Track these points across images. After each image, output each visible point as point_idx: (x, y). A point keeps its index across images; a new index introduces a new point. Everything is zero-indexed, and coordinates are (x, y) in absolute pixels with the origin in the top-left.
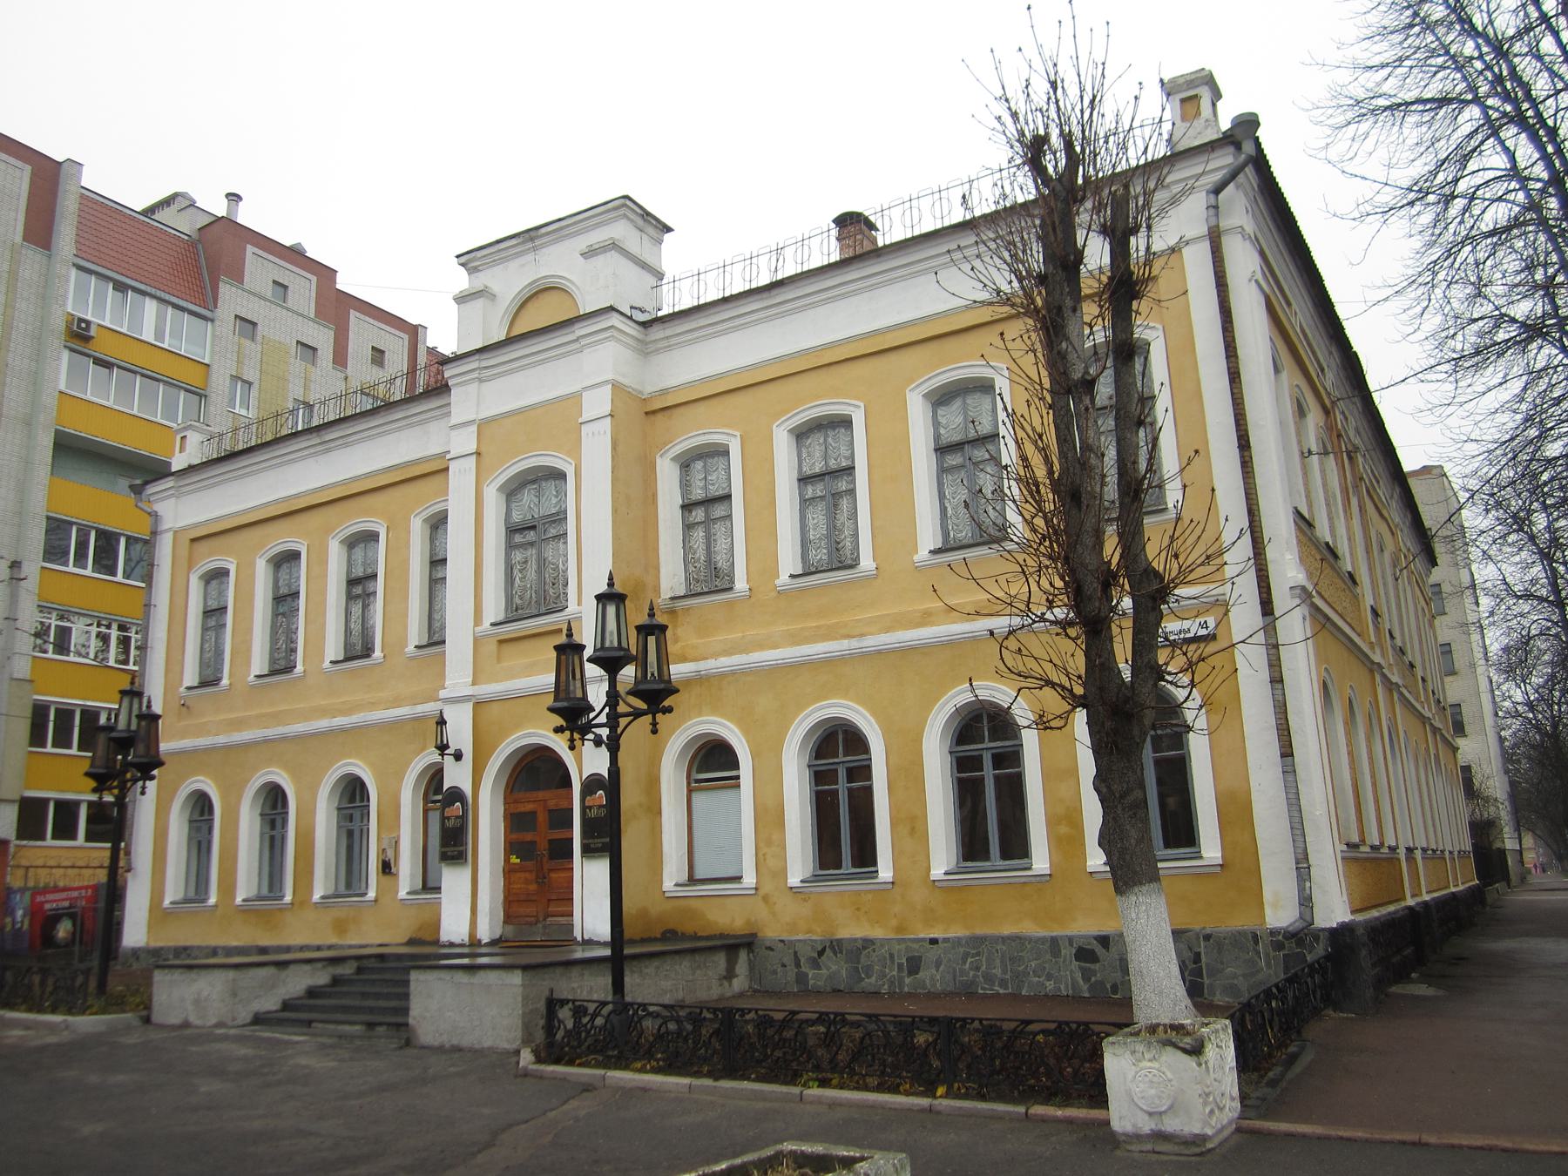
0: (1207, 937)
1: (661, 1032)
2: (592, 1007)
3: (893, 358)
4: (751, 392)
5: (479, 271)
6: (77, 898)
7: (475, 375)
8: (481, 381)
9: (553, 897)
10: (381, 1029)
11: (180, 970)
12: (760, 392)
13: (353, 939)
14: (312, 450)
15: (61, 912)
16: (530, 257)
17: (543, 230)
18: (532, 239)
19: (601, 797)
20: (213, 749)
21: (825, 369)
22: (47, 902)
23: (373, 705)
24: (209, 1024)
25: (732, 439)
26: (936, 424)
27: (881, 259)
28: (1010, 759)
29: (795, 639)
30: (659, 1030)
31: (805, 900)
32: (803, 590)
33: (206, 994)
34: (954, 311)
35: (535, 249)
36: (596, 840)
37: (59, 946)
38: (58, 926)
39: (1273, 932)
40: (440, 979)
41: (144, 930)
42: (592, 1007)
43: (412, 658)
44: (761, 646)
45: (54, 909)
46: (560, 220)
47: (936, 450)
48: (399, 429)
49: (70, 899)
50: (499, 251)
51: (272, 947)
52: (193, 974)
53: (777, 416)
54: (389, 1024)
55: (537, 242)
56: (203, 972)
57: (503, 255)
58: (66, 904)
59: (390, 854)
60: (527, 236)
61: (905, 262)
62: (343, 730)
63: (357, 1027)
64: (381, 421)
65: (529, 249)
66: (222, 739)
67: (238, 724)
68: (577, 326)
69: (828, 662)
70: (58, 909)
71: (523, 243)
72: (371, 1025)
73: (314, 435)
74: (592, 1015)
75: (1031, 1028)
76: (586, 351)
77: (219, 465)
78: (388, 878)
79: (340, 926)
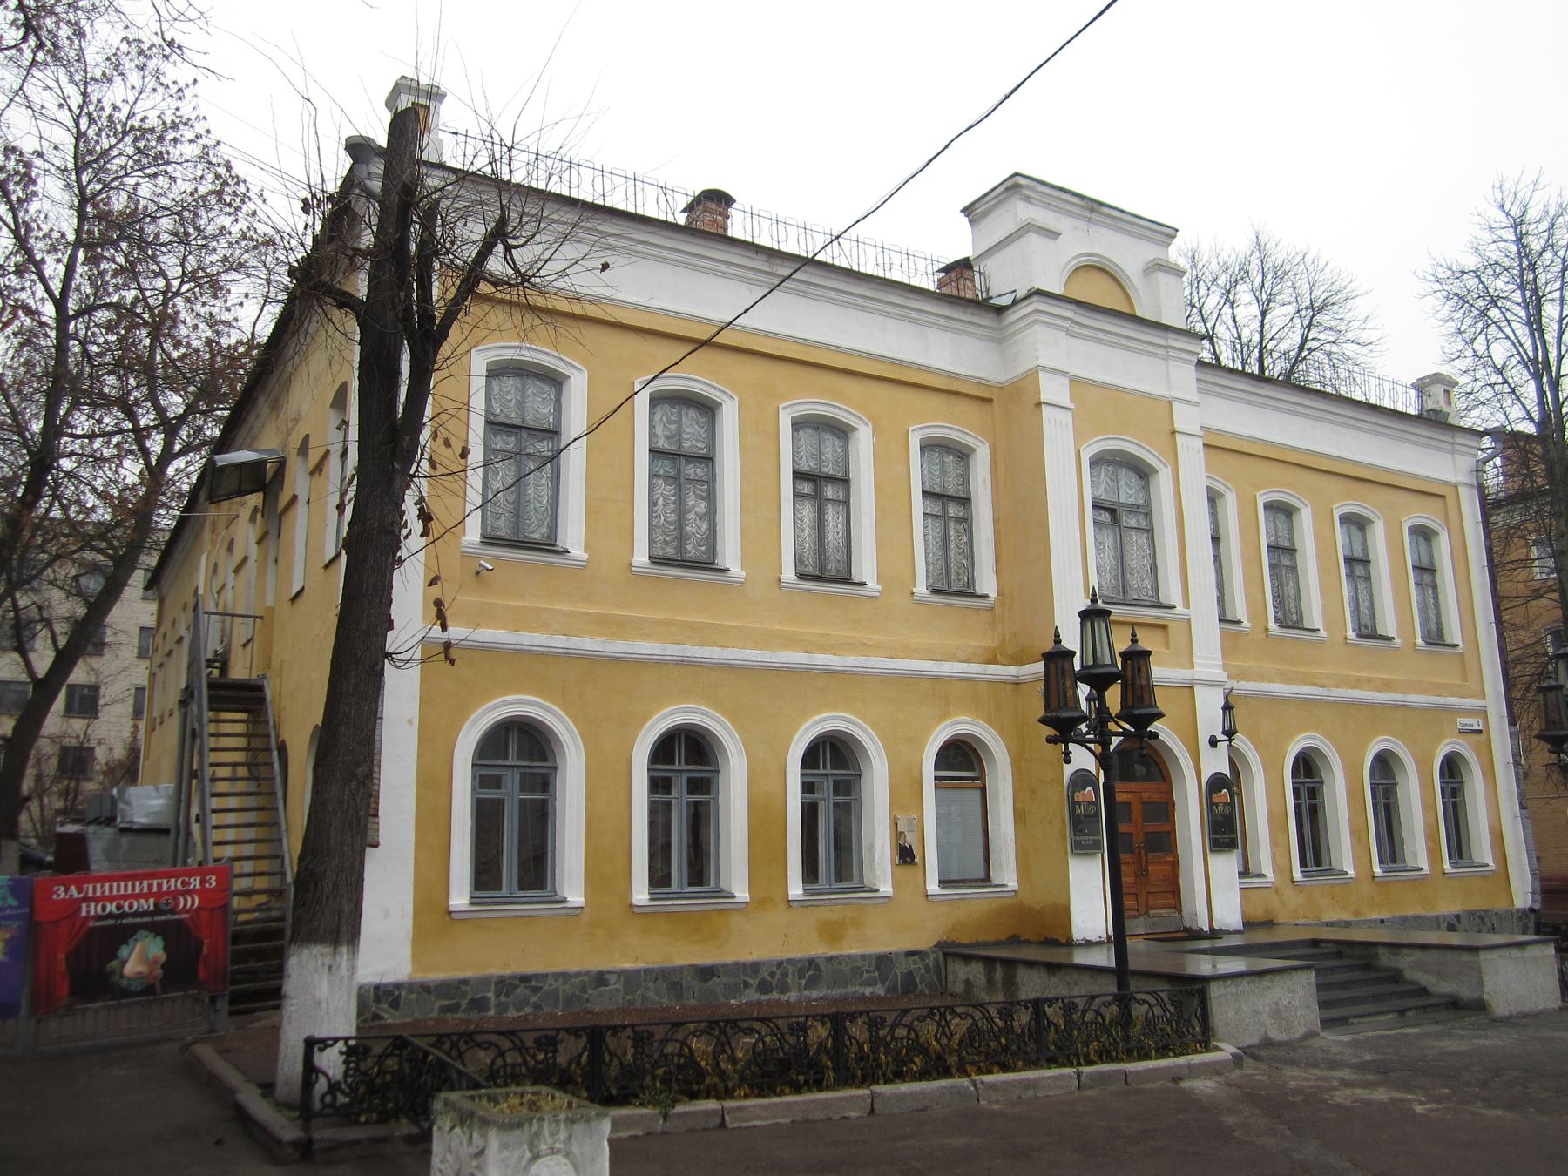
0: (1496, 914)
1: (495, 1067)
2: (1081, 1003)
3: (1322, 477)
4: (1239, 457)
5: (1030, 202)
6: (175, 894)
7: (1066, 324)
8: (1069, 333)
9: (1153, 889)
10: (1409, 1014)
11: (1247, 979)
12: (1246, 460)
13: (852, 947)
14: (749, 275)
15: (130, 920)
16: (1083, 225)
17: (1105, 210)
18: (1092, 210)
19: (1089, 793)
20: (565, 656)
21: (1311, 472)
22: (86, 899)
23: (867, 648)
24: (1297, 1036)
25: (576, 372)
26: (1290, 530)
27: (1326, 401)
28: (543, 781)
29: (1287, 680)
30: (493, 1062)
31: (1301, 892)
32: (1282, 638)
33: (1285, 1003)
34: (913, 366)
35: (1090, 220)
36: (1087, 838)
37: (125, 993)
38: (124, 951)
39: (1518, 910)
40: (1501, 956)
41: (406, 952)
42: (890, 1018)
43: (920, 603)
44: (1261, 678)
45: (111, 915)
46: (1123, 211)
47: (1369, 562)
48: (887, 315)
49: (159, 895)
50: (1059, 199)
51: (724, 966)
52: (1266, 981)
53: (1260, 487)
54: (1416, 1008)
55: (1094, 216)
56: (1278, 977)
57: (1061, 205)
58: (150, 905)
59: (911, 839)
60: (1090, 203)
61: (659, 243)
62: (828, 673)
63: (1390, 1016)
64: (868, 293)
65: (1085, 217)
66: (588, 644)
67: (620, 627)
68: (1170, 335)
69: (1307, 703)
70: (124, 915)
71: (1083, 207)
72: (1401, 1012)
73: (764, 258)
74: (892, 1027)
75: (1097, 1001)
76: (1172, 363)
77: (1299, 394)
78: (907, 870)
79: (831, 932)
